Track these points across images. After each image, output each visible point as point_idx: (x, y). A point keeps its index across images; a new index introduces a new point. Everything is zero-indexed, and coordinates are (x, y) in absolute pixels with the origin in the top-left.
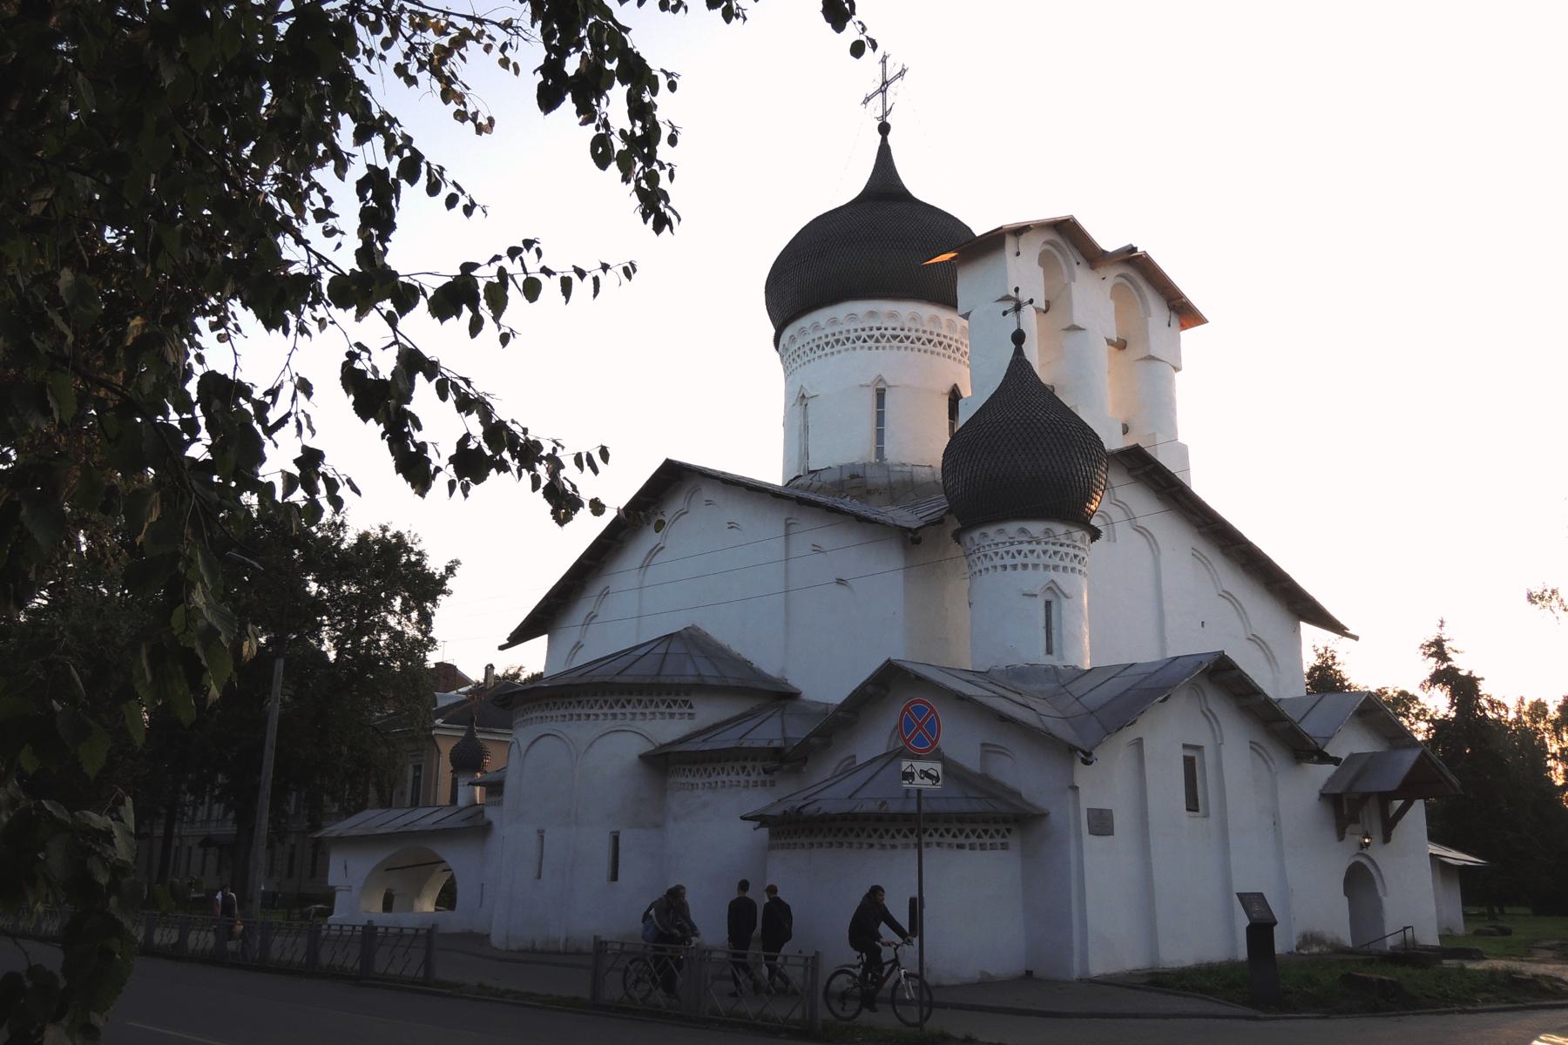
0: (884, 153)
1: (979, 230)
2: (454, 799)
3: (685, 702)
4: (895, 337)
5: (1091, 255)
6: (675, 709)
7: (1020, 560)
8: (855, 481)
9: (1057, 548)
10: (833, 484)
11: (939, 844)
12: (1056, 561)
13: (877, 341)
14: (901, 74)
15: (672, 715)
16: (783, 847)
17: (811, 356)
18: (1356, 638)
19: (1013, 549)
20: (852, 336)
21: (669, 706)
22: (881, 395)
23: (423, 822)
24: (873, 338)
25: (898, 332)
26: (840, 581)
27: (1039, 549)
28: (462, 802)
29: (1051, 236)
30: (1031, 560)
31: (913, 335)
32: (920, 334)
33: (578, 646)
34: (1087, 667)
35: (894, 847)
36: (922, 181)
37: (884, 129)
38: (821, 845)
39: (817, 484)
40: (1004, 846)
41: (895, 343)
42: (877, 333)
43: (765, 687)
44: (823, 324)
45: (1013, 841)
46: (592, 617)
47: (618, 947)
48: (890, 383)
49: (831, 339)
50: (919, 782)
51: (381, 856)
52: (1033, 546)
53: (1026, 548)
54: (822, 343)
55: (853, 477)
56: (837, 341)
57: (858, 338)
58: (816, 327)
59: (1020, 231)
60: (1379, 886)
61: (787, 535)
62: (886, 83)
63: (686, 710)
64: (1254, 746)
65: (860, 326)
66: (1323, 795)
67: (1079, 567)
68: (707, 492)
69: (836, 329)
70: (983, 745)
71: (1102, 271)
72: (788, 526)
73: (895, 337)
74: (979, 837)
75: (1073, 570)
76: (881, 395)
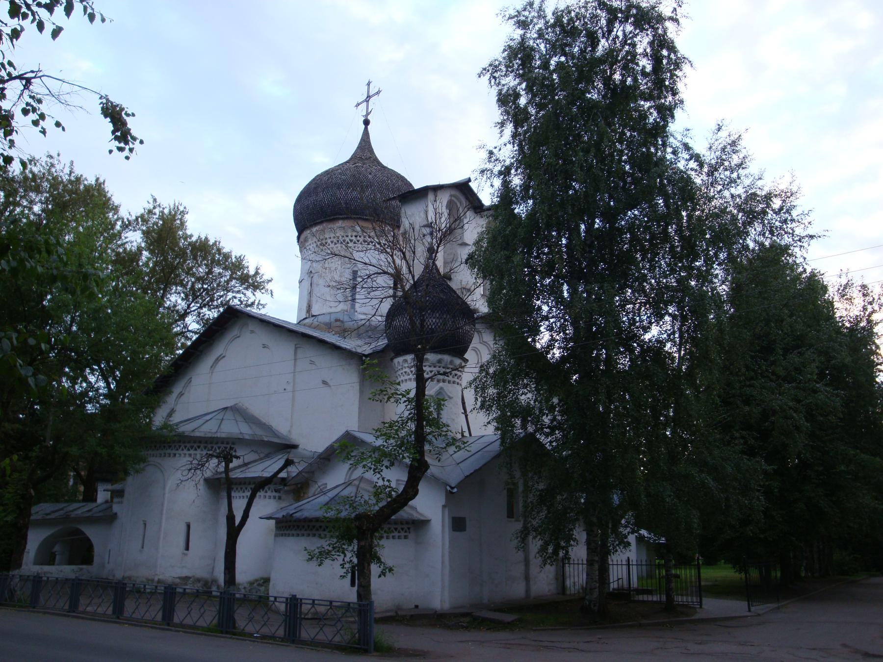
0: (366, 134)
1: (416, 186)
8: (338, 323)
14: (378, 93)
16: (282, 535)
23: (76, 512)
36: (388, 155)
37: (366, 123)
38: (303, 535)
40: (406, 537)
45: (411, 535)
46: (181, 394)
51: (328, 487)
55: (337, 320)
59: (436, 189)
61: (295, 360)
62: (369, 97)
67: (457, 381)
68: (252, 326)
72: (296, 349)
75: (454, 382)
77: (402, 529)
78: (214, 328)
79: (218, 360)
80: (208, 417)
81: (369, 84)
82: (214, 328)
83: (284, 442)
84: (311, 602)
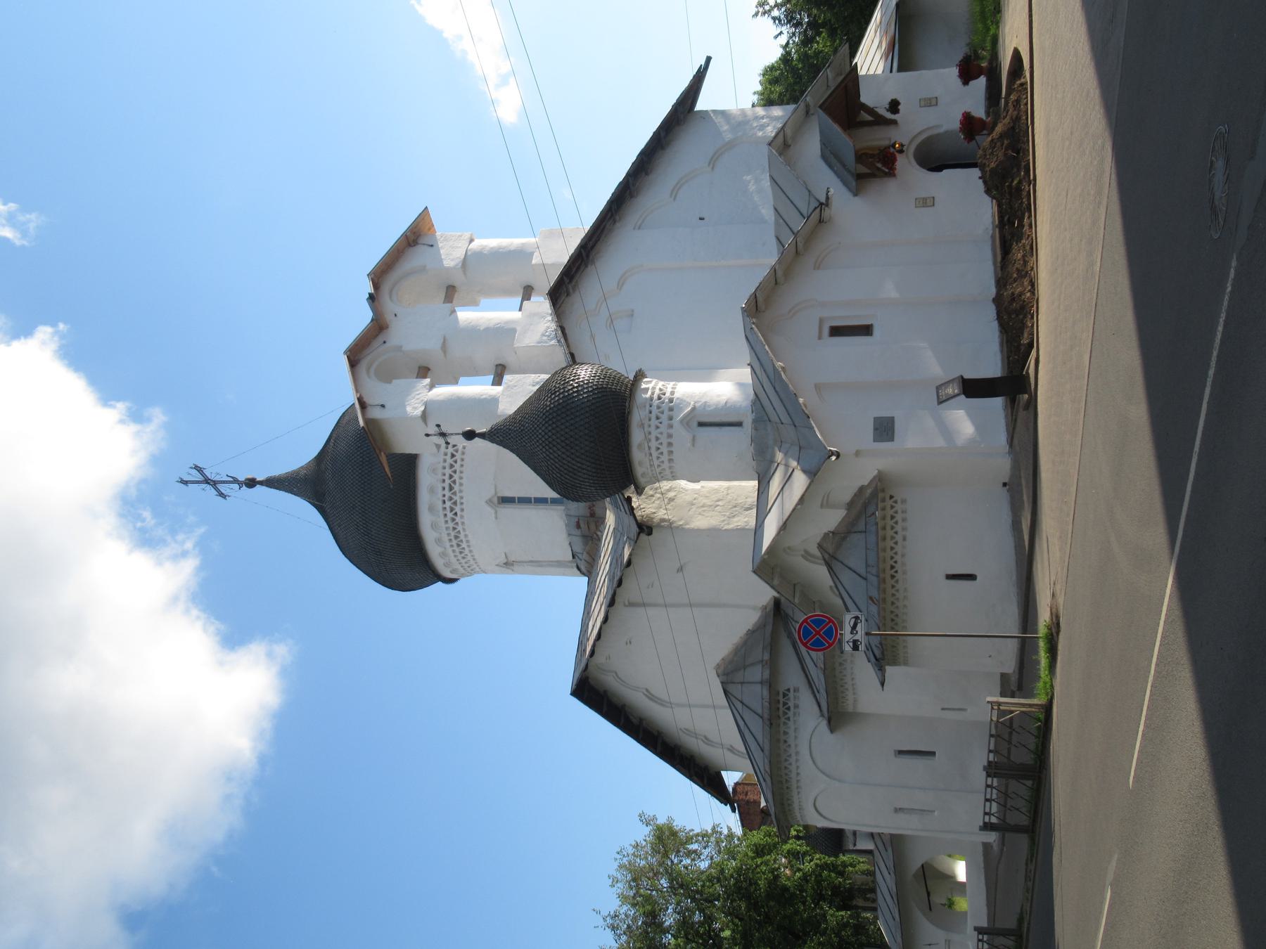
0: (272, 483)
2: (870, 852)
3: (785, 695)
4: (451, 488)
5: (378, 327)
6: (791, 704)
7: (664, 449)
9: (653, 416)
10: (586, 544)
11: (903, 556)
12: (664, 418)
13: (455, 503)
14: (222, 495)
15: (796, 706)
17: (469, 558)
18: (709, 59)
19: (655, 454)
20: (451, 525)
21: (789, 709)
22: (506, 500)
24: (453, 508)
25: (446, 485)
26: (681, 569)
27: (654, 433)
28: (870, 846)
29: (362, 367)
30: (664, 440)
31: (448, 471)
32: (447, 465)
33: (732, 750)
34: (749, 370)
35: (906, 590)
36: (302, 450)
37: (251, 483)
39: (585, 556)
41: (456, 488)
42: (448, 504)
43: (769, 628)
44: (440, 550)
47: (991, 756)
48: (493, 492)
49: (454, 542)
50: (860, 635)
52: (653, 437)
53: (654, 444)
54: (457, 550)
55: (578, 526)
56: (456, 537)
57: (453, 520)
58: (443, 555)
60: (935, 132)
61: (644, 605)
63: (791, 695)
64: (817, 267)
65: (442, 519)
66: (855, 195)
69: (446, 538)
70: (822, 506)
71: (389, 317)
72: (632, 605)
73: (451, 488)
74: (896, 523)
76: (506, 500)
77: (892, 507)
78: (605, 709)
79: (652, 697)
80: (742, 723)
81: (185, 483)
82: (605, 709)
83: (771, 620)
84: (988, 804)
